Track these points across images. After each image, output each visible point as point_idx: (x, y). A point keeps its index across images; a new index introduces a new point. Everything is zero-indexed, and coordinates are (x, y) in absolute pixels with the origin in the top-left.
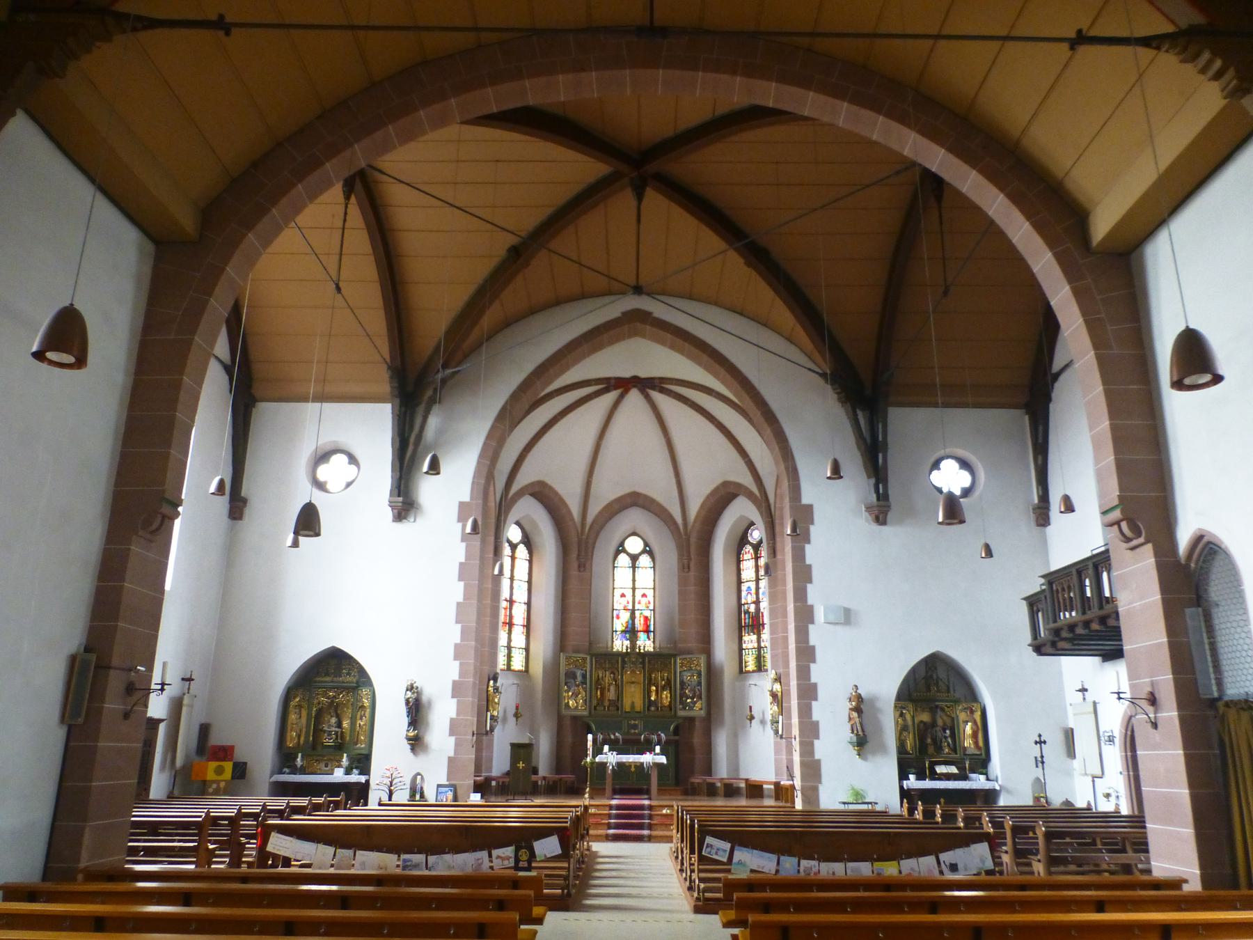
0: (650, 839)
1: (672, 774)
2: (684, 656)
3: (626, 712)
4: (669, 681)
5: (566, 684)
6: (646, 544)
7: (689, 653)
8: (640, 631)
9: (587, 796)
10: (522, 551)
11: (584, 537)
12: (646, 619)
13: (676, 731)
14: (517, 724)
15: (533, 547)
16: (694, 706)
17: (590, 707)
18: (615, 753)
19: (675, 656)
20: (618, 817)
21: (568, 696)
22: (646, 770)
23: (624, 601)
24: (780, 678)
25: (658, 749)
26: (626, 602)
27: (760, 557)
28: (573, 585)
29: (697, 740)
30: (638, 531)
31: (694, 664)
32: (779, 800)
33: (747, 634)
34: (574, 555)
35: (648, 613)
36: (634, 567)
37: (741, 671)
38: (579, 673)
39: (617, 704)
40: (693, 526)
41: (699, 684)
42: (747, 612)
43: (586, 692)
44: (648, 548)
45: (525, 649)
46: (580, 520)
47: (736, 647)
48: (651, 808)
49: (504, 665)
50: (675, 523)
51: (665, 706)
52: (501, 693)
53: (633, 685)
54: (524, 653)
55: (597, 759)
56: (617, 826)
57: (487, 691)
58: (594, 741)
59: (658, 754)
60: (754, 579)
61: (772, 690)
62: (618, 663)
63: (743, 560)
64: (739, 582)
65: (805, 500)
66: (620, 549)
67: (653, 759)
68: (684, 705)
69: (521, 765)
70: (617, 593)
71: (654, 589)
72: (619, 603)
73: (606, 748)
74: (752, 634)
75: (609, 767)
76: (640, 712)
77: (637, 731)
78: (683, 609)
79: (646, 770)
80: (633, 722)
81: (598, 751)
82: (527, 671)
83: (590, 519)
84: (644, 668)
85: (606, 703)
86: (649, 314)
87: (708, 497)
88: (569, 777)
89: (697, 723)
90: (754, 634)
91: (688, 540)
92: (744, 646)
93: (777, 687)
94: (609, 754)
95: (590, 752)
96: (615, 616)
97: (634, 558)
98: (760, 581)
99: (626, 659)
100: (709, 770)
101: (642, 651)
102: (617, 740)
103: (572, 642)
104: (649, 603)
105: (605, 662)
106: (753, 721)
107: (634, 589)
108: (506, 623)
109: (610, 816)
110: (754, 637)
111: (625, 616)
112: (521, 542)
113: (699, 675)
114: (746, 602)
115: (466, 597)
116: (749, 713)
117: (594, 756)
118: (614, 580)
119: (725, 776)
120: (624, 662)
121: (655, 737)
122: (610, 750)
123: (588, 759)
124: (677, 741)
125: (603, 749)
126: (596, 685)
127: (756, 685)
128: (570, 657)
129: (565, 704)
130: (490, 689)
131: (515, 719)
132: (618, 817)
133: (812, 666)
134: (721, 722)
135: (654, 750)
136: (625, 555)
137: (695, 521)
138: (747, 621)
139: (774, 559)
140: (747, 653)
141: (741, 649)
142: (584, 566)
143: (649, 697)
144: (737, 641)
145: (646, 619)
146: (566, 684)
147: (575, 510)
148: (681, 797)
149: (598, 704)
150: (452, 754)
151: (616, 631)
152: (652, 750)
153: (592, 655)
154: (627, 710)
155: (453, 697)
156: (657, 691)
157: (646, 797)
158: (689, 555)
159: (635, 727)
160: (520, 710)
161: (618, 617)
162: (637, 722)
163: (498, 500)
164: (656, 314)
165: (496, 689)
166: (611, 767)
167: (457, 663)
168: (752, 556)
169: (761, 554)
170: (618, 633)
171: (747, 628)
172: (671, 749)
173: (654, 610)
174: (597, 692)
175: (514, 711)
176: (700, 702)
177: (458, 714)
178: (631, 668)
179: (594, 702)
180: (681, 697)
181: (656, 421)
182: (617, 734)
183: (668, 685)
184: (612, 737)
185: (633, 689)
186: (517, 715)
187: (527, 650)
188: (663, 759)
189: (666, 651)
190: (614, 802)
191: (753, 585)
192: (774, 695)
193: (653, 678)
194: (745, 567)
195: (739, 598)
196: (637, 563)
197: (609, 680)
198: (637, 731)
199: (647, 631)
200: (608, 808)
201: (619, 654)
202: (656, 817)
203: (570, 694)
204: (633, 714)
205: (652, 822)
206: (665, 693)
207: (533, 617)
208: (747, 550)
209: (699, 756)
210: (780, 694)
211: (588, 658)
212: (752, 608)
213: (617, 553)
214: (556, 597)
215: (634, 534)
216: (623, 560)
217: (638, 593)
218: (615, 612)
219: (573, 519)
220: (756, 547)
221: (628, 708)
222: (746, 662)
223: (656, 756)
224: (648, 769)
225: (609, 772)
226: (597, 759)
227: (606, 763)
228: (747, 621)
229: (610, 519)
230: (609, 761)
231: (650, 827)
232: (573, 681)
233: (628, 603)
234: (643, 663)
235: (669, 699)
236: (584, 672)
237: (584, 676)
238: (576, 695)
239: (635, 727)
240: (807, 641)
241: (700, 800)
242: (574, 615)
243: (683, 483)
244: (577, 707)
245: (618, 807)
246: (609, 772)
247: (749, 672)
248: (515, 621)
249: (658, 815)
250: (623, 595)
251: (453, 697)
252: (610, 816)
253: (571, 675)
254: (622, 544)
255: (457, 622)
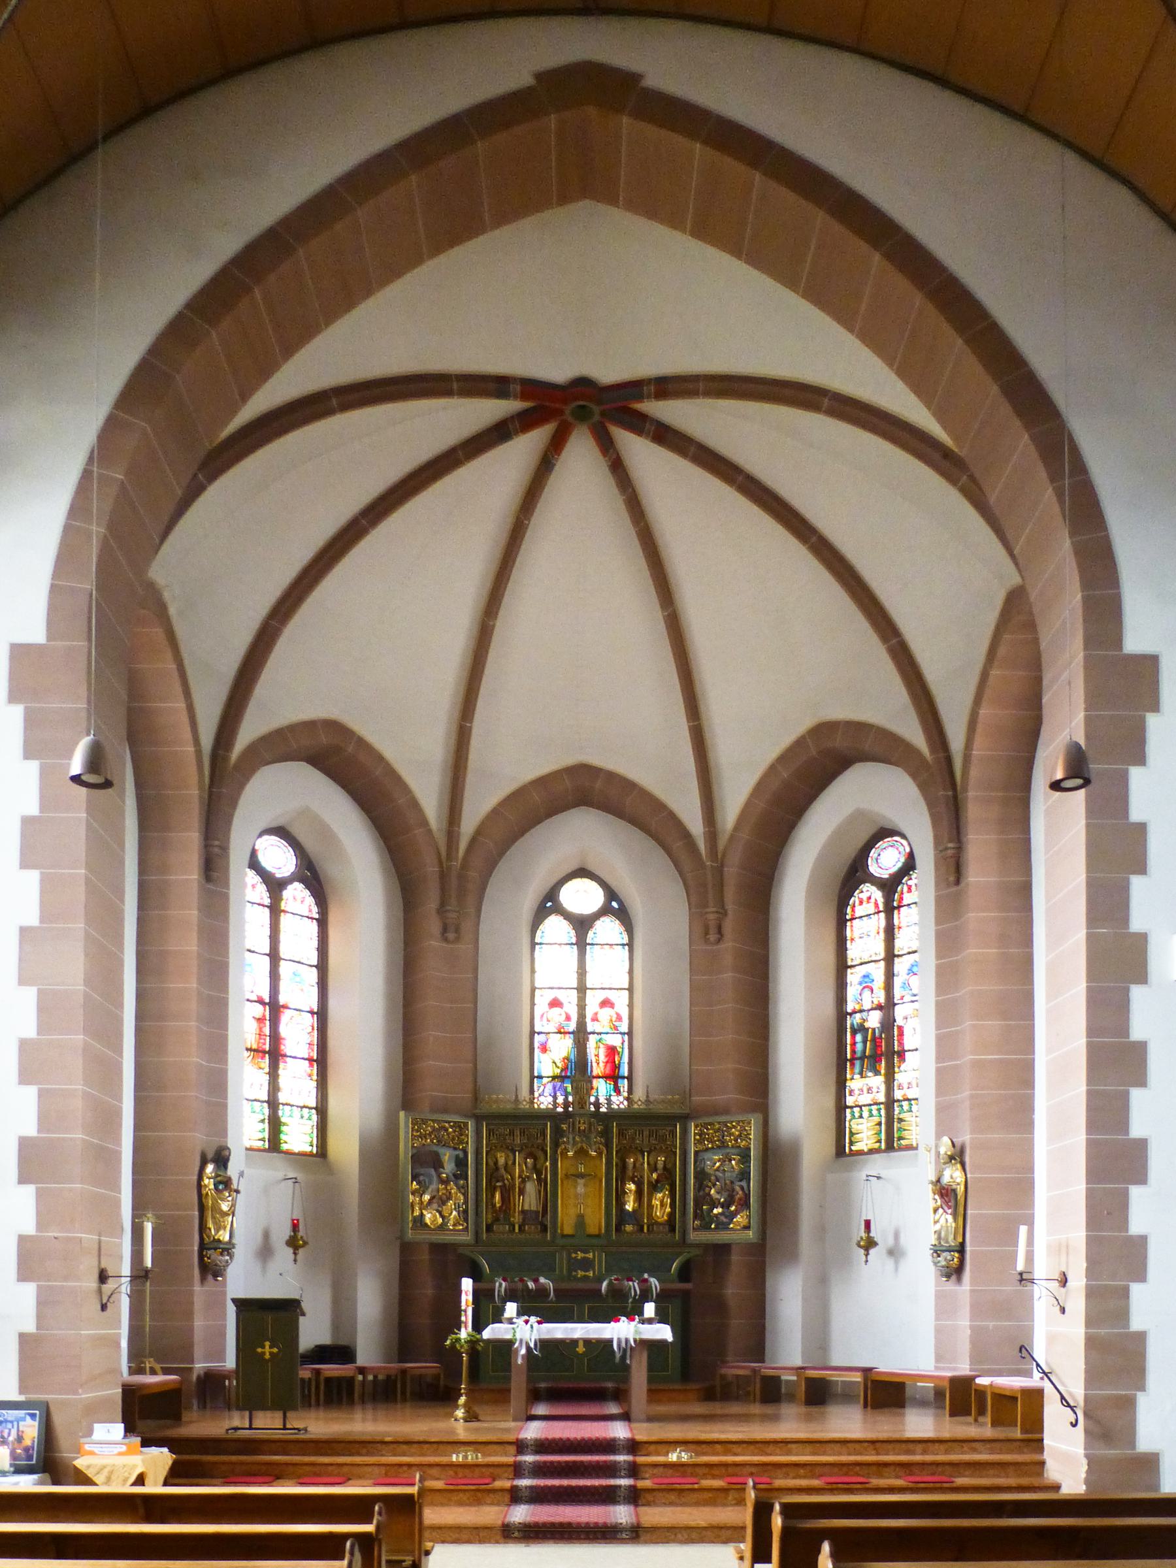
0: (636, 1534)
1: (674, 1360)
2: (707, 1120)
3: (564, 1236)
4: (668, 1173)
5: (415, 1177)
6: (611, 894)
7: (716, 1113)
8: (598, 1077)
9: (460, 1413)
10: (297, 898)
11: (457, 864)
12: (612, 1051)
13: (685, 1273)
14: (295, 1261)
15: (328, 890)
16: (731, 1221)
17: (477, 1224)
18: (533, 1319)
19: (685, 1119)
20: (540, 1470)
21: (421, 1202)
22: (618, 1356)
23: (557, 1015)
24: (962, 1152)
25: (649, 1309)
26: (564, 1017)
27: (899, 907)
28: (433, 969)
29: (733, 1289)
30: (591, 867)
31: (730, 1135)
32: (967, 1413)
33: (857, 1076)
34: (431, 904)
35: (615, 1040)
36: (581, 944)
37: (842, 1149)
38: (447, 1157)
39: (543, 1218)
40: (732, 838)
41: (744, 1175)
42: (861, 1029)
43: (465, 1195)
44: (615, 904)
45: (316, 1108)
46: (445, 824)
47: (830, 1103)
48: (633, 1446)
49: (263, 1140)
50: (686, 835)
51: (657, 1223)
52: (237, 1191)
53: (581, 1181)
54: (315, 1118)
55: (487, 1334)
56: (538, 1497)
57: (200, 1186)
58: (479, 1296)
59: (650, 1321)
60: (882, 955)
61: (938, 1181)
62: (544, 1134)
63: (852, 919)
64: (842, 966)
65: (1134, 642)
66: (549, 904)
67: (636, 1332)
68: (705, 1222)
69: (267, 1350)
70: (541, 1000)
71: (631, 989)
72: (547, 1020)
73: (511, 1309)
74: (870, 1074)
75: (517, 1351)
76: (598, 1236)
77: (591, 1274)
78: (700, 1023)
79: (618, 1356)
80: (580, 1255)
81: (487, 1311)
82: (322, 1151)
83: (469, 824)
84: (608, 1145)
85: (517, 1219)
86: (629, 80)
87: (772, 769)
88: (425, 1367)
89: (735, 1258)
90: (877, 1073)
91: (719, 871)
92: (850, 1101)
93: (953, 1175)
94: (520, 1321)
95: (468, 1317)
96: (536, 1045)
97: (582, 924)
98: (896, 960)
99: (564, 1127)
100: (757, 1346)
101: (603, 1110)
102: (542, 1292)
103: (430, 1090)
104: (619, 1018)
105: (512, 1133)
106: (872, 1251)
107: (582, 989)
108: (264, 1052)
109: (518, 1470)
110: (877, 1082)
111: (562, 1048)
112: (297, 877)
113: (745, 1156)
114: (857, 1007)
115: (48, 912)
116: (864, 1235)
117: (478, 1326)
118: (533, 971)
119: (798, 1362)
120: (558, 1133)
121: (635, 1286)
122: (520, 1313)
123: (464, 1334)
124: (686, 1294)
125: (502, 1310)
126: (489, 1182)
127: (878, 1178)
128: (424, 1121)
129: (415, 1220)
130: (206, 1181)
131: (291, 1250)
132: (540, 1470)
133: (1136, 1094)
134: (791, 1254)
135: (641, 1313)
136: (561, 918)
137: (738, 827)
138: (859, 1047)
139: (954, 889)
140: (857, 1115)
141: (841, 1108)
142: (457, 930)
143: (621, 1204)
144: (832, 1089)
145: (612, 1051)
146: (415, 1177)
147: (430, 801)
148: (699, 1408)
149: (496, 1220)
150: (30, 1327)
151: (540, 1077)
152: (634, 1312)
153: (479, 1119)
154: (566, 1232)
155: (23, 1179)
156: (639, 1193)
157: (613, 1409)
158: (721, 903)
159: (586, 1264)
160: (301, 1233)
161: (544, 1049)
162: (590, 1255)
163: (207, 739)
164: (653, 81)
165: (224, 1184)
166: (523, 1351)
167: (31, 1093)
168: (876, 905)
169: (901, 899)
170: (545, 1080)
171: (858, 1063)
172: (673, 1308)
173: (630, 1033)
174: (493, 1196)
175: (287, 1232)
176: (745, 1213)
177: (41, 1224)
178: (575, 1143)
179: (486, 1217)
180: (698, 1204)
181: (646, 573)
182: (542, 1280)
183: (667, 1178)
184: (531, 1285)
185: (580, 1189)
186: (294, 1243)
187: (322, 1110)
188: (664, 1332)
189: (661, 1109)
190: (533, 1431)
191: (878, 972)
192: (945, 1193)
193: (631, 1166)
194: (856, 935)
195: (841, 999)
196: (590, 934)
197: (521, 1171)
198: (591, 1274)
199: (613, 1076)
200: (513, 1449)
201: (548, 1115)
202: (650, 1471)
203: (427, 1197)
204: (582, 1238)
205: (641, 1484)
206: (660, 1195)
207: (332, 1043)
208: (864, 896)
209: (737, 1324)
210: (961, 1190)
211: (471, 1124)
212: (874, 1020)
213: (541, 914)
214: (390, 997)
215: (582, 872)
216: (555, 929)
217: (593, 1000)
218: (538, 1039)
219: (424, 823)
220: (890, 886)
221: (568, 1230)
222: (852, 1134)
223: (646, 1326)
224: (623, 1357)
225: (520, 1361)
226: (487, 1334)
227: (510, 1343)
228: (859, 1047)
229: (523, 831)
230: (518, 1336)
231: (634, 1497)
232: (432, 1171)
233: (568, 1018)
234: (606, 1134)
235: (668, 1210)
236: (461, 1155)
237: (461, 1163)
238: (440, 1201)
239: (586, 1264)
240: (1123, 1028)
241: (745, 1418)
242: (432, 1036)
243: (707, 735)
244: (444, 1224)
245: (542, 1446)
246: (520, 1361)
247: (860, 1153)
248: (288, 1047)
249: (655, 1465)
250: (555, 1003)
251: (23, 1179)
252: (518, 1470)
253: (425, 1161)
254: (552, 895)
255: (23, 981)
